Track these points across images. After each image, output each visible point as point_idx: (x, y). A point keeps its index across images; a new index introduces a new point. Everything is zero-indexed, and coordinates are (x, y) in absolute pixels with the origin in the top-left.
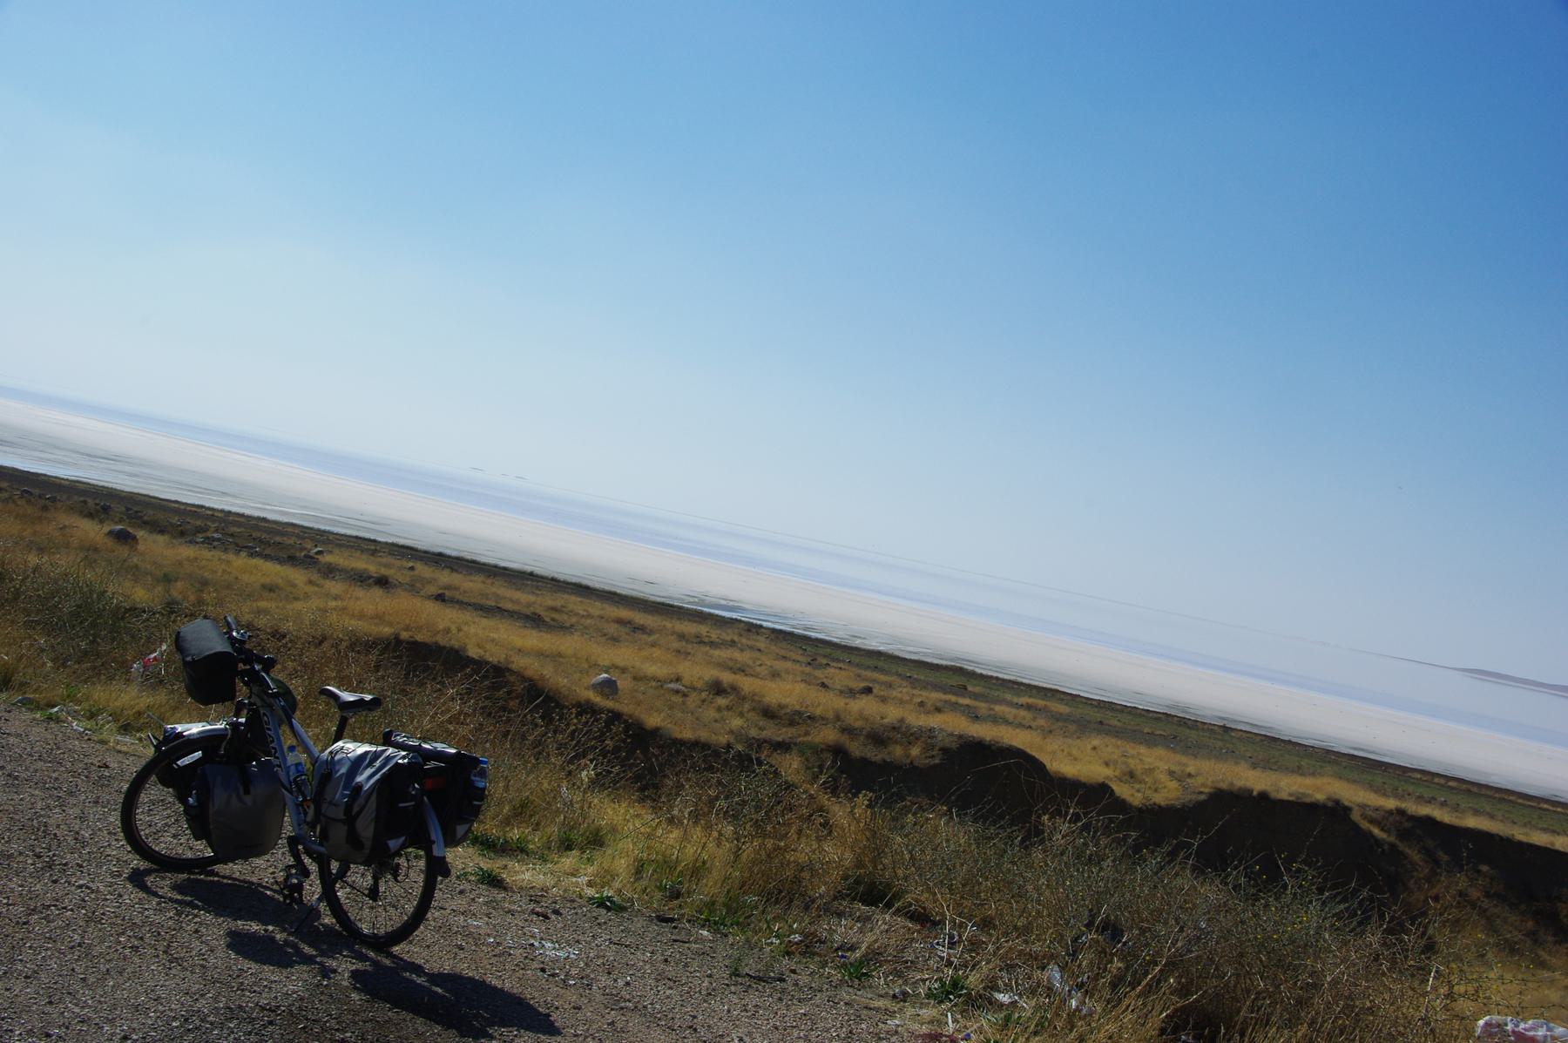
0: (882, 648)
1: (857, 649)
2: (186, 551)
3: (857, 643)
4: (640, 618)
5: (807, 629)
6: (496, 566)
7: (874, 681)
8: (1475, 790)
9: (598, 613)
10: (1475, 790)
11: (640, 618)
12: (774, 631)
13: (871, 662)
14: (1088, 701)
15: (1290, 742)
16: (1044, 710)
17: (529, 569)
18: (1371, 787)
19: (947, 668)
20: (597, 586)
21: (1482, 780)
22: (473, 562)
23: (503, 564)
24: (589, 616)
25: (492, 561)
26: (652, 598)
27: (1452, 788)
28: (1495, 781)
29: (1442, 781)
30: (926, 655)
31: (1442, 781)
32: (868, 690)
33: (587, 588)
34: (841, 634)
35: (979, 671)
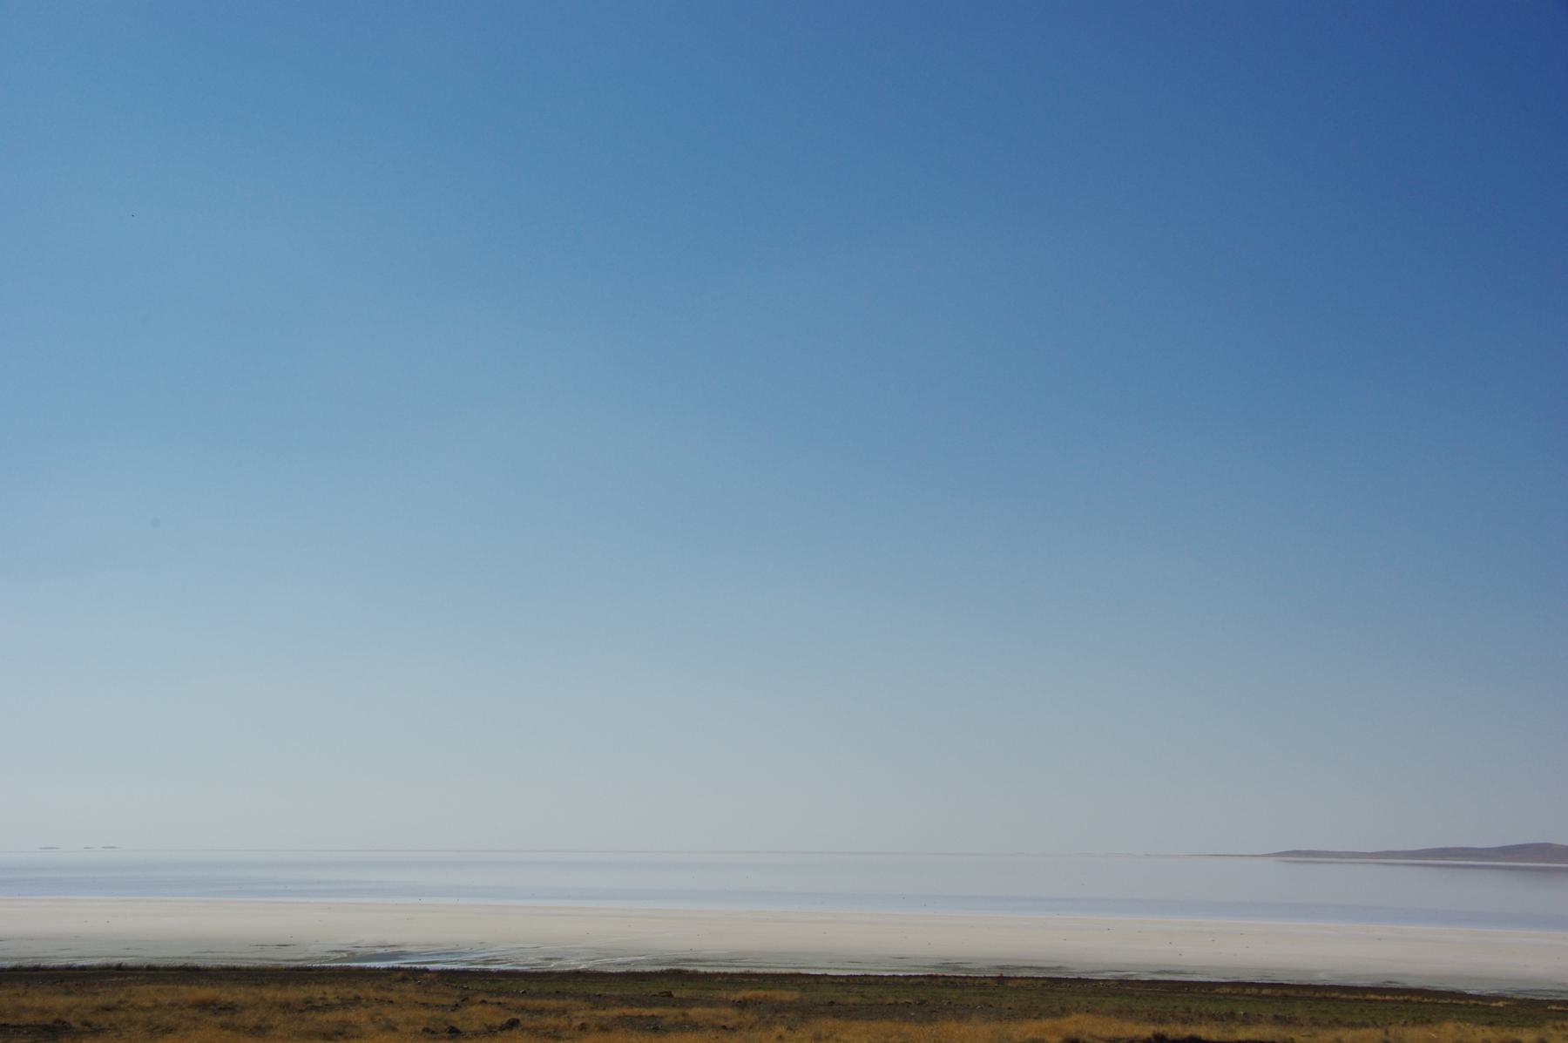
0: (583, 967)
1: (550, 974)
2: (714, 1011)
3: (553, 966)
4: (224, 994)
5: (488, 962)
6: (69, 968)
7: (523, 1009)
8: (1293, 993)
9: (168, 999)
10: (1293, 993)
11: (224, 994)
12: (442, 973)
13: (534, 988)
14: (879, 980)
15: (1079, 980)
16: (756, 1003)
17: (115, 961)
18: (1119, 1013)
19: (662, 974)
20: (210, 964)
21: (1305, 980)
22: (37, 969)
23: (80, 963)
24: (157, 1006)
25: (63, 962)
26: (285, 964)
27: (1267, 996)
28: (1321, 978)
29: (1255, 991)
30: (638, 963)
31: (1255, 991)
32: (513, 1024)
33: (197, 970)
34: (532, 959)
35: (702, 970)
